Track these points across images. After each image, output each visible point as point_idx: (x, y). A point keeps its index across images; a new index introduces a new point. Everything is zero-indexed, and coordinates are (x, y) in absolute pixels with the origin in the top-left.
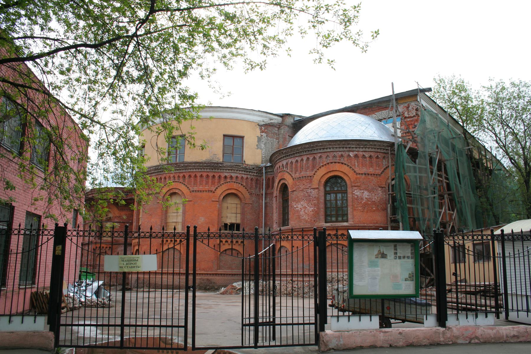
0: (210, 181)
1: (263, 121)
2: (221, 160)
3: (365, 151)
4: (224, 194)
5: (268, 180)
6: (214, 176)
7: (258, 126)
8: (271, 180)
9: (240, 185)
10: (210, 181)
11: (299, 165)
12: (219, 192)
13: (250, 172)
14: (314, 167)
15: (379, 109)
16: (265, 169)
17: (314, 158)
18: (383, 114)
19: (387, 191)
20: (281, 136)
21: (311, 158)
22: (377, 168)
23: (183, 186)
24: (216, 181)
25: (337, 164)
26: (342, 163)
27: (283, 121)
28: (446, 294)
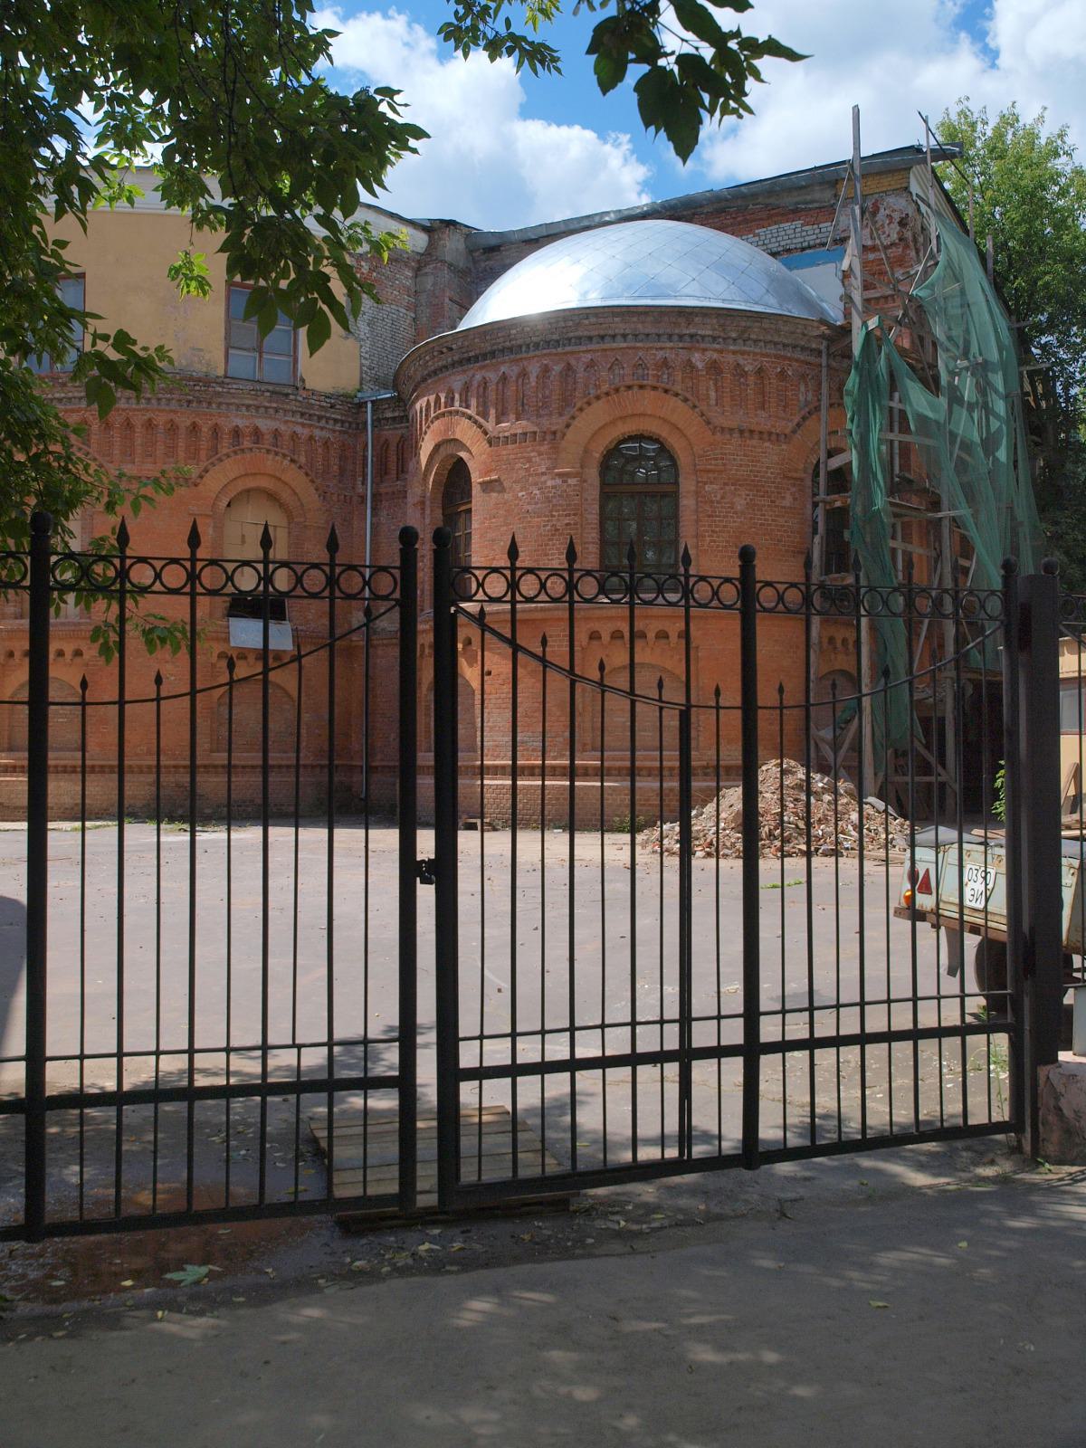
0: (181, 444)
2: (221, 372)
3: (743, 353)
4: (242, 485)
5: (382, 448)
6: (194, 428)
8: (393, 448)
9: (286, 462)
10: (181, 444)
11: (511, 390)
13: (320, 418)
14: (566, 401)
15: (770, 217)
16: (373, 411)
17: (569, 367)
18: (790, 232)
20: (423, 298)
21: (557, 368)
24: (204, 444)
25: (649, 394)
27: (432, 244)
28: (1060, 830)
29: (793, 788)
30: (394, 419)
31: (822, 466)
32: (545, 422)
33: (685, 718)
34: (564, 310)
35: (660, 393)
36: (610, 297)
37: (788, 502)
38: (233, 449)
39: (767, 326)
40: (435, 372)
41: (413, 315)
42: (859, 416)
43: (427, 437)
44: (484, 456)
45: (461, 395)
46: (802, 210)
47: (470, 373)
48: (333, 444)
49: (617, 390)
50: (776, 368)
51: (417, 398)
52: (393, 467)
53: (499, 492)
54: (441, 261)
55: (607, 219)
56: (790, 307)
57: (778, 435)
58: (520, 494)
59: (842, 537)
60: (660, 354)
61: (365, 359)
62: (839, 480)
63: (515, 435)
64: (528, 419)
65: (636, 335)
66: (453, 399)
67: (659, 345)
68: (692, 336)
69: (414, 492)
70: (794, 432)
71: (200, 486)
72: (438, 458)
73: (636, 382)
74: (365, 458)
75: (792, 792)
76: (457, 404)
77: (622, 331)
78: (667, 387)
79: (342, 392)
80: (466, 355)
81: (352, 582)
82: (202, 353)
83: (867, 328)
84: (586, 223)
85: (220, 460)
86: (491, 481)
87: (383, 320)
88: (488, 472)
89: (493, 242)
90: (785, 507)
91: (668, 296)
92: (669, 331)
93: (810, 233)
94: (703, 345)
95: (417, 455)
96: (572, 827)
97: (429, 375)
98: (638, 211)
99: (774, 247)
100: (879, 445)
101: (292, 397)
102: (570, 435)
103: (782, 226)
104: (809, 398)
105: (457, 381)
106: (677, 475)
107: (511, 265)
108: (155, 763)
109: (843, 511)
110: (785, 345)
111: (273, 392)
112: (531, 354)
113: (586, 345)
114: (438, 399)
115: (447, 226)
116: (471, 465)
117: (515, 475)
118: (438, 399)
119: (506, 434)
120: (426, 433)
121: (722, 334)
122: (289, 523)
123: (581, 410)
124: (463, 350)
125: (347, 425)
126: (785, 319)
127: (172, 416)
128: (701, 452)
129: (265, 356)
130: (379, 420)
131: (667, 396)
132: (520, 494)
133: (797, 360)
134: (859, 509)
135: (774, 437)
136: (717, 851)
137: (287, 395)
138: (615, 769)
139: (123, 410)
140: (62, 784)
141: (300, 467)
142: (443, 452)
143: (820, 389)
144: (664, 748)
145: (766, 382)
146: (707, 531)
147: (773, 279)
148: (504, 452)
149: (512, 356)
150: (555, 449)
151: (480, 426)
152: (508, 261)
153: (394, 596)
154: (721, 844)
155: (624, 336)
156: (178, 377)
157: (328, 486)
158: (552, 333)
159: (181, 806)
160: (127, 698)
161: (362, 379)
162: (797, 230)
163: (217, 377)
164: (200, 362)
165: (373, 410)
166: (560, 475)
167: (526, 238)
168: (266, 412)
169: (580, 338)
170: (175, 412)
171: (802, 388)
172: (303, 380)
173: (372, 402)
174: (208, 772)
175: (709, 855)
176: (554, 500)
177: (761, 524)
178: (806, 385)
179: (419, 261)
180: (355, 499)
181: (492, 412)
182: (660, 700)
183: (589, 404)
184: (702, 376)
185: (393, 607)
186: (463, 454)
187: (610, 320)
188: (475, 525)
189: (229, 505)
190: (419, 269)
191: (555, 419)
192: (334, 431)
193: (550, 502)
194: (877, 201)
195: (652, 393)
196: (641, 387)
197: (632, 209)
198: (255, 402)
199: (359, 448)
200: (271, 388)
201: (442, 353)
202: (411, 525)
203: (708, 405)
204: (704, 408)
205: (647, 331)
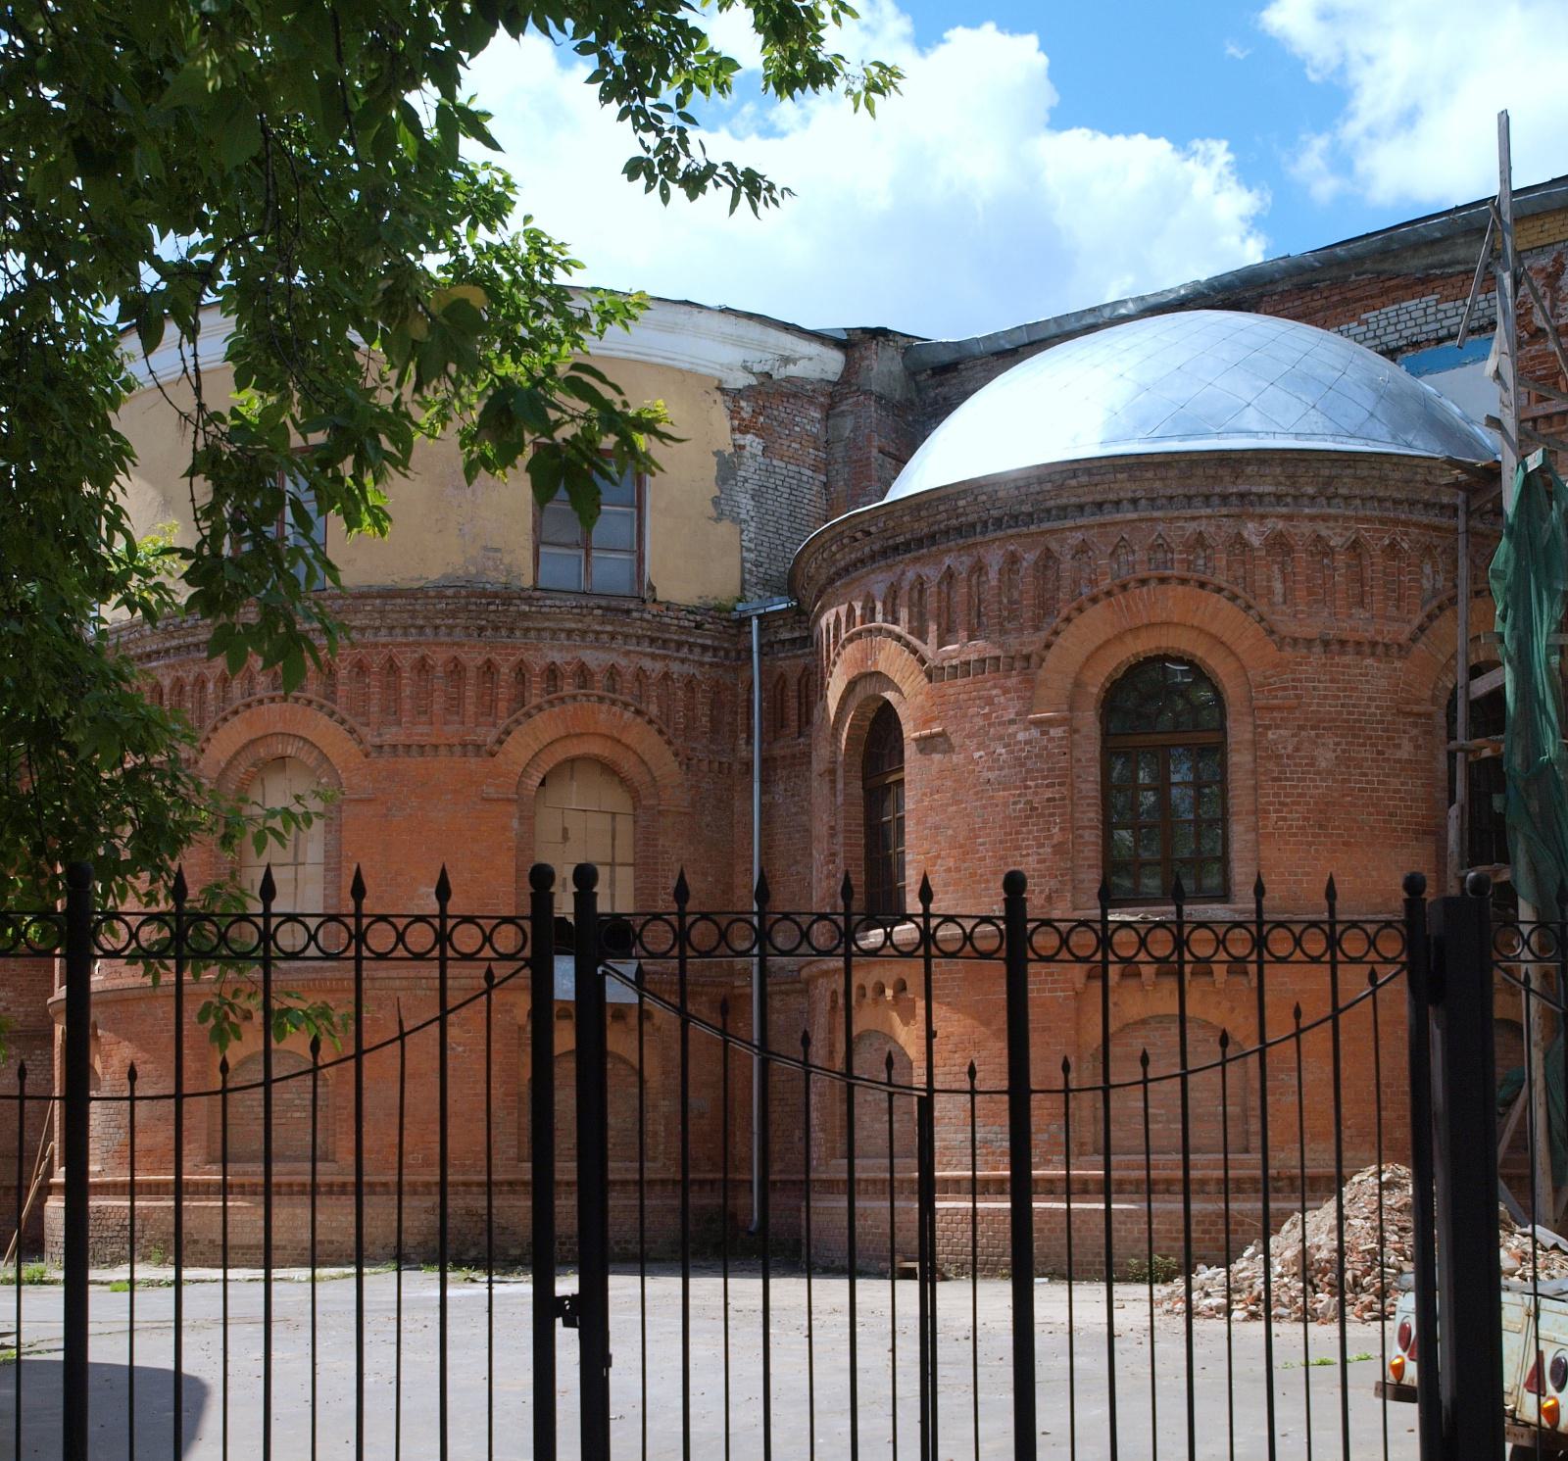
0: (470, 692)
1: (746, 368)
2: (527, 581)
3: (1325, 518)
4: (561, 753)
5: (775, 689)
6: (489, 668)
7: (718, 396)
9: (628, 715)
10: (470, 692)
11: (961, 591)
12: (520, 749)
13: (679, 645)
14: (1045, 606)
15: (1385, 292)
17: (1048, 553)
18: (1415, 314)
19: (1443, 733)
21: (1030, 557)
22: (1392, 612)
23: (323, 719)
24: (503, 692)
26: (1202, 585)
29: (1399, 1210)
30: (793, 641)
31: (1460, 693)
32: (1013, 642)
33: (926, 1106)
34: (1038, 466)
35: (1191, 589)
36: (1115, 441)
37: (1406, 751)
38: (547, 698)
39: (1365, 473)
40: (846, 570)
41: (823, 478)
42: (1516, 611)
43: (836, 670)
44: (920, 698)
45: (884, 604)
46: (1437, 277)
47: (898, 570)
48: (700, 683)
49: (1124, 587)
50: (1381, 539)
51: (823, 610)
52: (793, 716)
53: (945, 752)
54: (865, 393)
55: (1123, 311)
56: (1410, 438)
57: (1386, 645)
58: (977, 755)
59: (1490, 805)
60: (1191, 527)
61: (749, 550)
62: (1489, 712)
63: (968, 663)
64: (986, 638)
65: (1153, 500)
66: (873, 610)
67: (1189, 513)
68: (1242, 496)
69: (821, 755)
70: (1413, 639)
71: (500, 757)
72: (854, 703)
73: (1154, 573)
74: (750, 702)
75: (1397, 1216)
76: (879, 617)
77: (1130, 495)
78: (1203, 578)
79: (713, 603)
80: (891, 542)
81: (466, 938)
82: (499, 555)
83: (1525, 468)
84: (1089, 320)
85: (529, 715)
86: (932, 736)
87: (776, 489)
88: (926, 723)
89: (946, 357)
90: (1399, 761)
91: (1205, 434)
92: (1205, 490)
93: (1453, 315)
94: (1259, 510)
95: (824, 697)
96: (1111, 1275)
97: (839, 575)
98: (1172, 296)
99: (1391, 340)
100: (1548, 656)
101: (635, 615)
102: (1051, 656)
103: (1403, 305)
104: (1439, 585)
105: (878, 582)
106: (1223, 716)
107: (974, 391)
108: (437, 1178)
109: (1496, 761)
110: (1396, 502)
111: (607, 609)
112: (990, 536)
113: (1074, 518)
114: (851, 611)
115: (874, 338)
116: (902, 712)
117: (967, 726)
118: (851, 611)
119: (954, 662)
120: (835, 663)
121: (1292, 491)
122: (635, 809)
123: (1068, 620)
124: (888, 534)
125: (722, 653)
126: (1395, 460)
127: (454, 651)
128: (1260, 679)
129: (595, 554)
130: (771, 645)
131: (1204, 593)
132: (977, 755)
133: (1417, 525)
134: (1517, 760)
135: (1380, 650)
136: (1268, 1309)
137: (628, 612)
138: (1131, 1182)
139: (385, 645)
140: (299, 1211)
141: (650, 722)
142: (861, 692)
143: (1456, 568)
144: (1230, 1149)
145: (1366, 562)
146: (1271, 803)
147: (1386, 396)
148: (951, 691)
149: (961, 541)
150: (1029, 682)
151: (914, 651)
152: (970, 387)
153: (522, 955)
154: (1273, 1299)
155: (1134, 501)
156: (463, 592)
157: (693, 749)
158: (1022, 503)
159: (475, 1245)
160: (185, 1091)
161: (743, 581)
162: (1429, 311)
163: (523, 590)
164: (496, 569)
165: (760, 629)
166: (1037, 723)
167: (995, 347)
168: (597, 639)
169: (1064, 508)
170: (460, 645)
171: (1428, 569)
172: (652, 588)
173: (759, 617)
174: (514, 1192)
175: (1253, 1316)
176: (1029, 763)
177: (1361, 790)
178: (1434, 564)
179: (831, 395)
180: (736, 767)
181: (933, 628)
182: (889, 1083)
183: (1080, 610)
184: (1261, 558)
185: (522, 968)
186: (889, 695)
187: (1111, 477)
188: (909, 804)
189: (543, 783)
190: (831, 407)
191: (1028, 636)
192: (702, 664)
193: (1022, 765)
194: (1560, 255)
195: (1180, 588)
196: (1163, 580)
197: (1161, 294)
198: (580, 625)
199: (741, 689)
200: (603, 603)
201: (856, 540)
202: (544, 861)
203: (1271, 604)
204: (1264, 609)
205: (1169, 492)
